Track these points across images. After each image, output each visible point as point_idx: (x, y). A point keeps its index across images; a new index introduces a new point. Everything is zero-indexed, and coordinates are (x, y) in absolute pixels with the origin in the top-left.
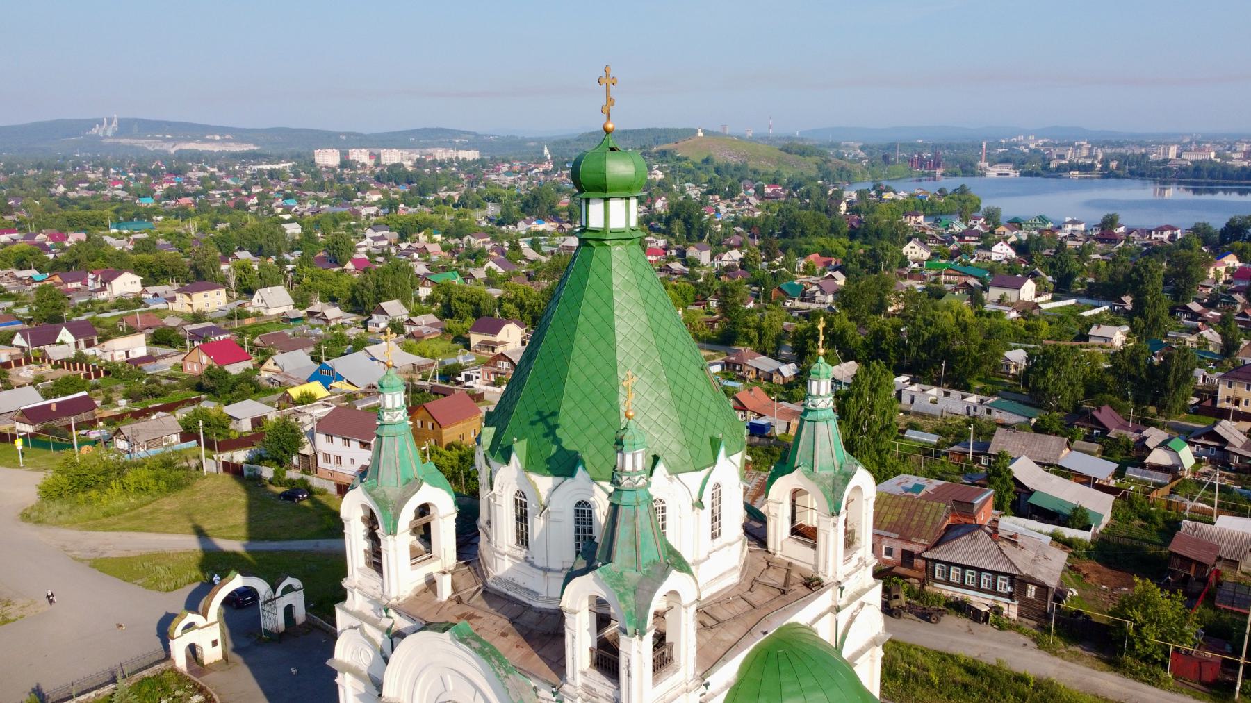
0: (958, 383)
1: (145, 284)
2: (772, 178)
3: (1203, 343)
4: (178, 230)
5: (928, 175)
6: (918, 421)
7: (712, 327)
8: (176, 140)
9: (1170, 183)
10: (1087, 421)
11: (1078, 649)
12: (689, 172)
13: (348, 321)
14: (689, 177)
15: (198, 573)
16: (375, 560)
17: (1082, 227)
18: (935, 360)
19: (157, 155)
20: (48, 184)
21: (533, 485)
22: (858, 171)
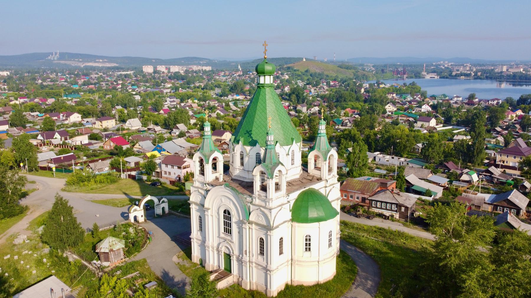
0: (399, 154)
1: (82, 118)
2: (334, 78)
3: (498, 143)
4: (91, 98)
5: (401, 77)
6: (381, 167)
7: (306, 135)
8: (84, 62)
9: (503, 81)
10: (443, 167)
11: (417, 227)
12: (299, 76)
13: (163, 132)
14: (299, 78)
15: (129, 202)
16: (202, 172)
17: (461, 99)
18: (389, 146)
19: (76, 68)
20: (34, 79)
21: (245, 149)
22: (370, 75)
